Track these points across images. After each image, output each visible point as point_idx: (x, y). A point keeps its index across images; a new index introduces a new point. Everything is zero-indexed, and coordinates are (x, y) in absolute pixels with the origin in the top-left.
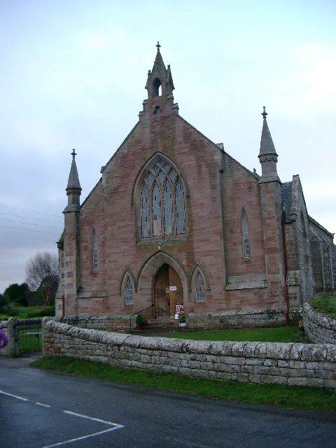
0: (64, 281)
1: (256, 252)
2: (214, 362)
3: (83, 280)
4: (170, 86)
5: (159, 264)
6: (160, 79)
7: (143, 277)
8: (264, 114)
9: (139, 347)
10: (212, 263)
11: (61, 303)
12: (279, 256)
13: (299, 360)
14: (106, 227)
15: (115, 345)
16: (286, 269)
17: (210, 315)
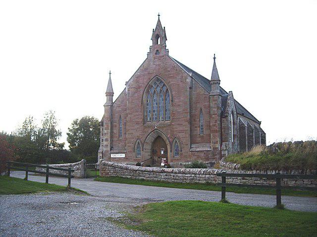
0: (103, 143)
1: (206, 132)
2: (174, 176)
3: (114, 143)
4: (165, 38)
5: (156, 136)
6: (159, 34)
7: (146, 142)
8: (215, 58)
9: (145, 171)
10: (185, 137)
11: (101, 155)
12: (218, 134)
13: (203, 174)
14: (127, 115)
15: (134, 170)
16: (222, 141)
17: (181, 164)
